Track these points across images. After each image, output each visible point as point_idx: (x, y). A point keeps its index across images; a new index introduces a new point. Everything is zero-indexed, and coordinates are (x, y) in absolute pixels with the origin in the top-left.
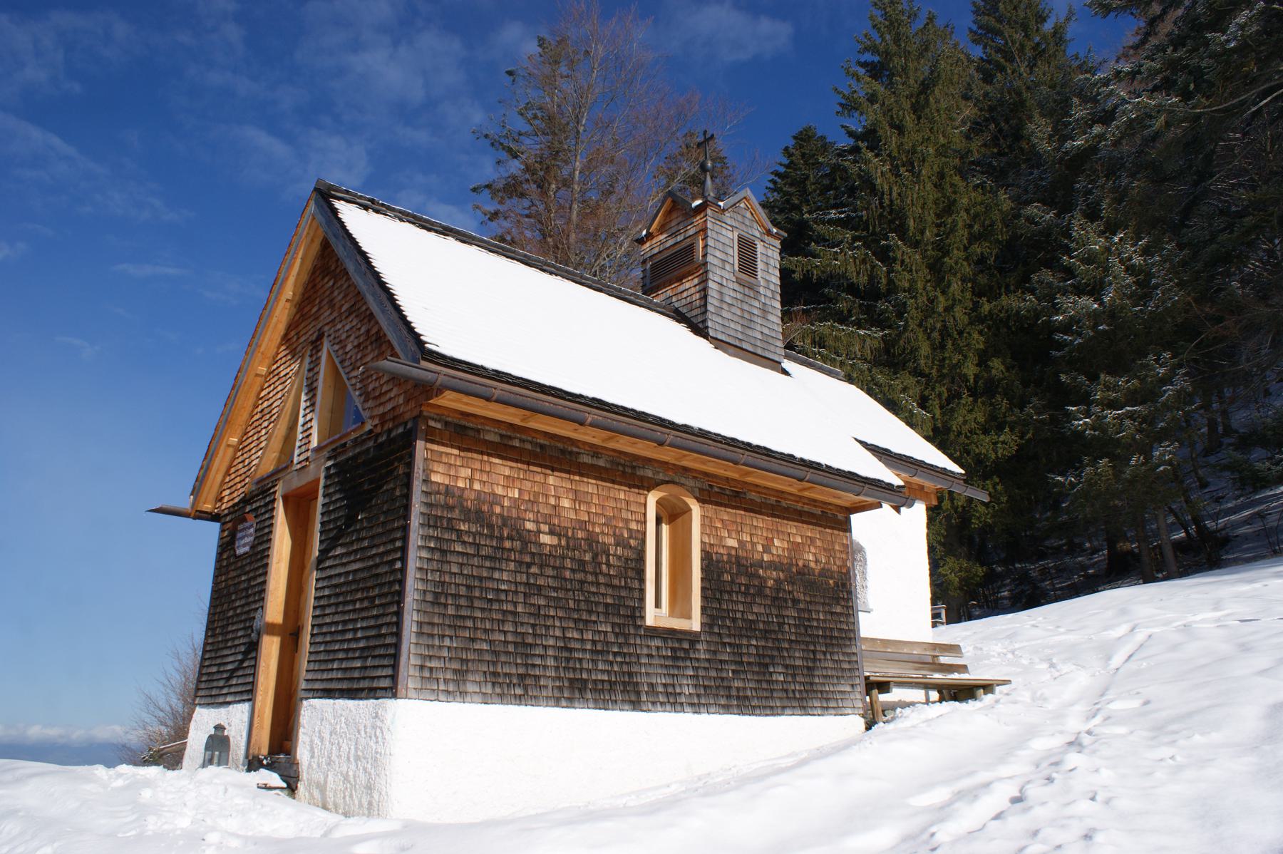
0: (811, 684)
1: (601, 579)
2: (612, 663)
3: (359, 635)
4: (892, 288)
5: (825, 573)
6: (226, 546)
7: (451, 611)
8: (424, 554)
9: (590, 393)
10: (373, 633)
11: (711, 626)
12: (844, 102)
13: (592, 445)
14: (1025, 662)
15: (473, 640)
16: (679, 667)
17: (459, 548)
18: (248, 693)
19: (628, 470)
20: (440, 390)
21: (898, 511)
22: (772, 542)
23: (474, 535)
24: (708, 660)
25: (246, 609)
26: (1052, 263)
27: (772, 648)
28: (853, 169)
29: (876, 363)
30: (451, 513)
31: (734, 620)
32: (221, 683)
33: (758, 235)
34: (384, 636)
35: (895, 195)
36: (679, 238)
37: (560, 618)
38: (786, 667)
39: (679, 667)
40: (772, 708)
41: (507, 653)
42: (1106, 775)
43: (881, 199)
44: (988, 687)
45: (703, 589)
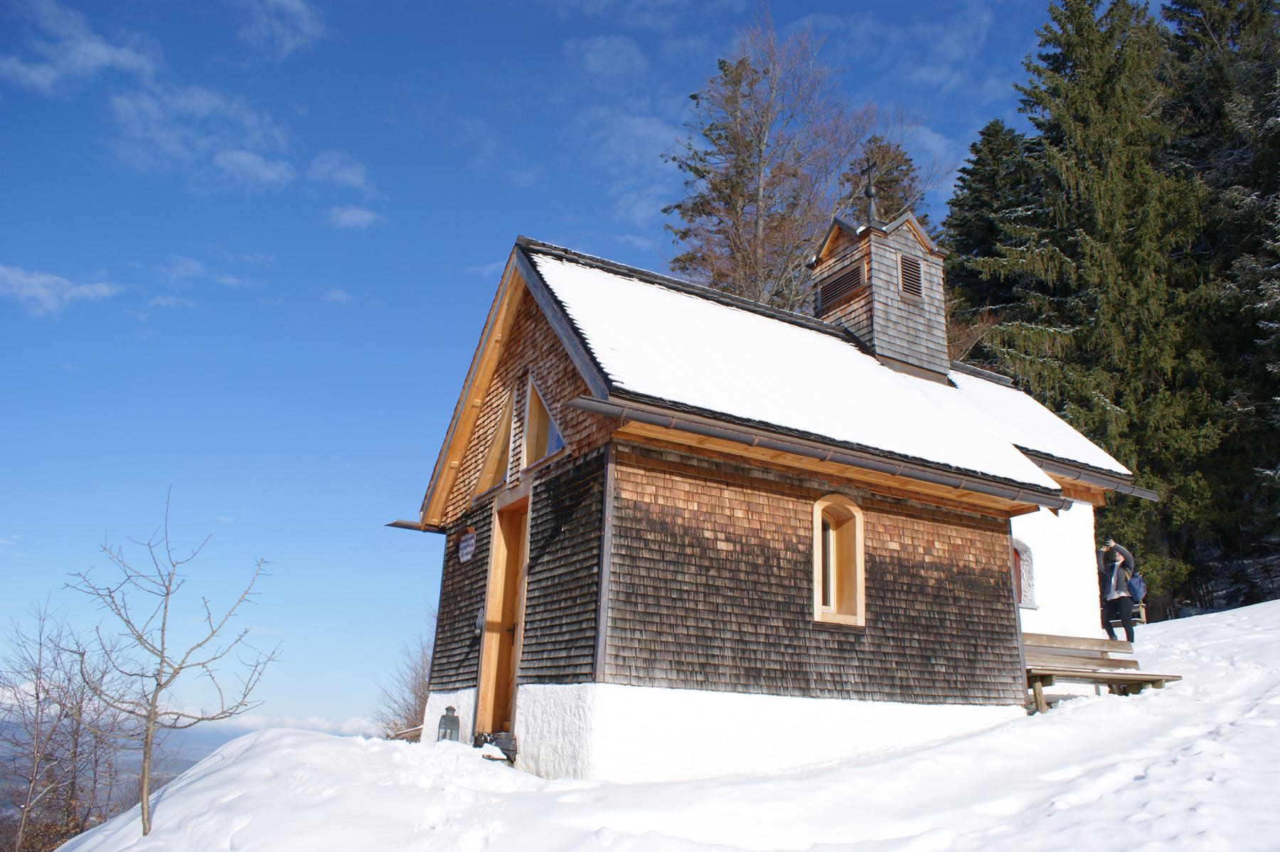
0: (973, 675)
1: (773, 581)
2: (783, 654)
3: (564, 629)
4: (1082, 284)
5: (985, 572)
6: (452, 554)
7: (641, 608)
8: (617, 560)
9: (757, 417)
10: (576, 627)
11: (875, 621)
12: (1025, 98)
13: (762, 462)
14: (1204, 659)
15: (660, 633)
16: (845, 659)
17: (646, 555)
18: (473, 680)
19: (796, 483)
20: (628, 419)
21: (1056, 514)
22: (933, 545)
23: (660, 543)
24: (872, 653)
25: (470, 608)
26: (1255, 249)
27: (933, 642)
28: (1038, 166)
29: (1067, 360)
30: (639, 525)
31: (897, 616)
32: (452, 672)
33: (921, 254)
34: (585, 630)
35: (1082, 188)
36: (847, 263)
37: (736, 615)
38: (948, 659)
39: (845, 659)
40: (934, 697)
41: (690, 645)
42: (1230, 759)
43: (1068, 193)
44: (1156, 682)
45: (867, 588)
